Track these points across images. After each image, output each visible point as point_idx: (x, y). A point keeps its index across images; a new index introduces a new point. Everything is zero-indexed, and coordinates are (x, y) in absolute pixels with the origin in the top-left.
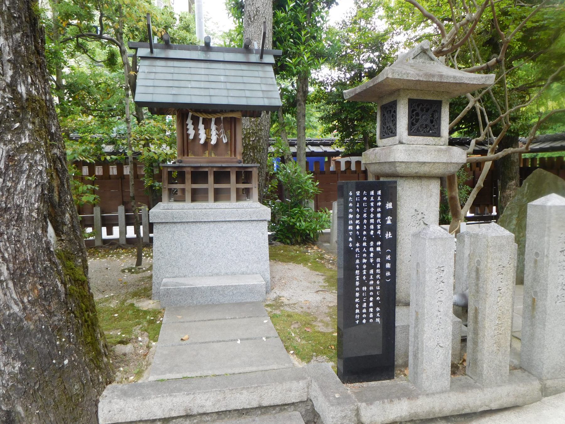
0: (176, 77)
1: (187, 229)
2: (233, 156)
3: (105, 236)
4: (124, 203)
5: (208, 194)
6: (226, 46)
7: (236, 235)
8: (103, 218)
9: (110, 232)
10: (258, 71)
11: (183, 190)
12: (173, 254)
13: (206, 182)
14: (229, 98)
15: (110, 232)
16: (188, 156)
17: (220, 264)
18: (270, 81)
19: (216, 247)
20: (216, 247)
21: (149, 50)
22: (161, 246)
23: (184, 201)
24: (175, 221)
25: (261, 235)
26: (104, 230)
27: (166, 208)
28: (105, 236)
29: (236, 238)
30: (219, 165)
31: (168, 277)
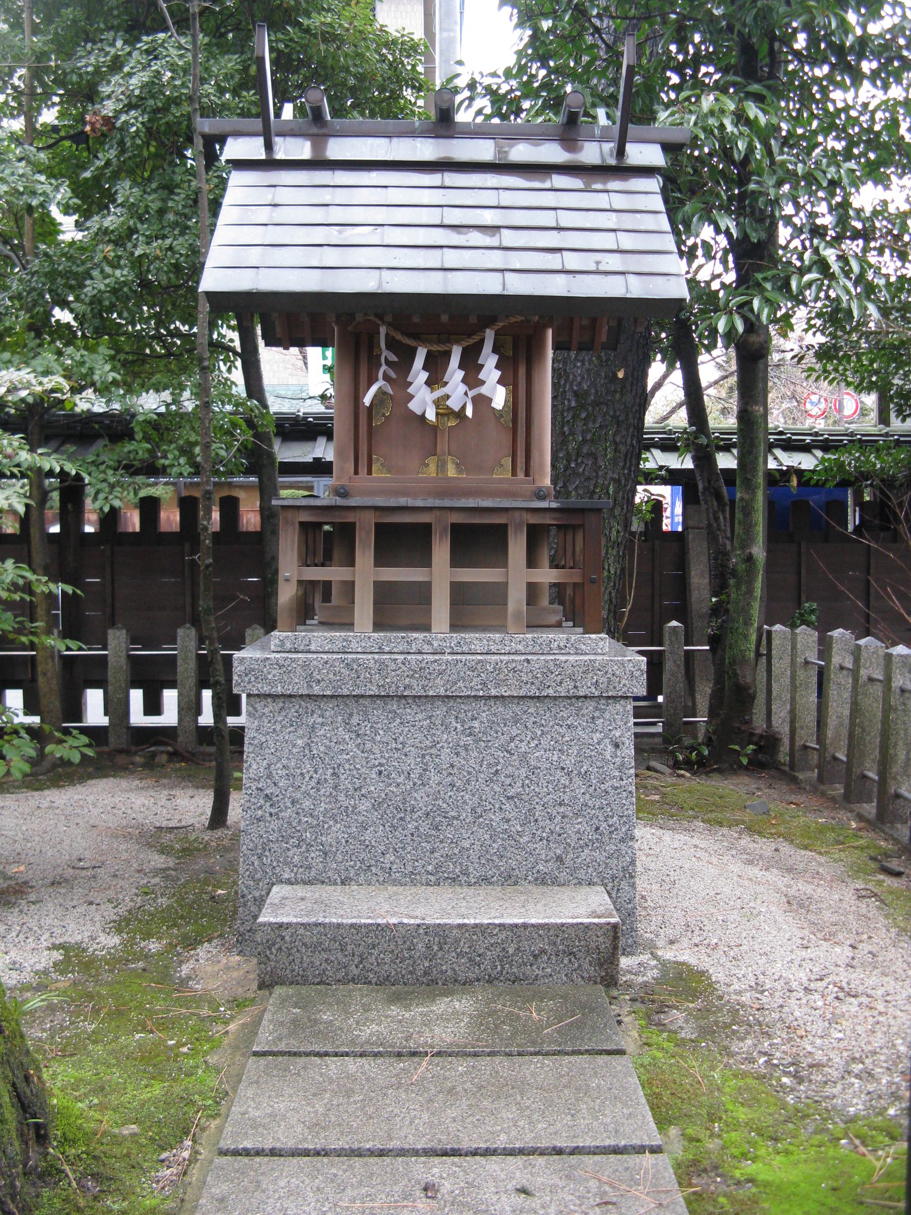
0: (337, 215)
1: (355, 720)
2: (521, 475)
3: (138, 717)
4: (195, 622)
5: (429, 603)
6: (824, 627)
7: (523, 747)
8: (134, 661)
9: (153, 706)
10: (614, 194)
11: (349, 586)
12: (307, 803)
13: (427, 562)
14: (508, 275)
15: (153, 706)
16: (370, 472)
17: (466, 844)
18: (648, 222)
19: (452, 785)
20: (452, 785)
21: (260, 141)
22: (270, 776)
23: (349, 625)
24: (317, 690)
25: (610, 748)
26: (136, 697)
27: (288, 646)
28: (138, 717)
29: (524, 757)
30: (471, 503)
31: (289, 882)
